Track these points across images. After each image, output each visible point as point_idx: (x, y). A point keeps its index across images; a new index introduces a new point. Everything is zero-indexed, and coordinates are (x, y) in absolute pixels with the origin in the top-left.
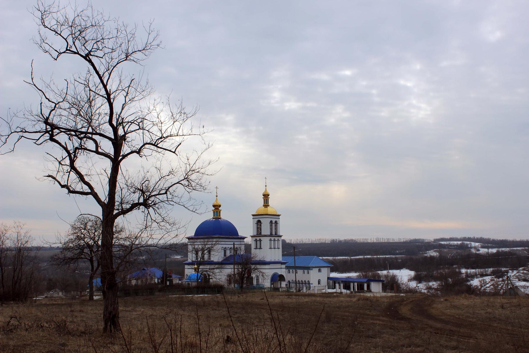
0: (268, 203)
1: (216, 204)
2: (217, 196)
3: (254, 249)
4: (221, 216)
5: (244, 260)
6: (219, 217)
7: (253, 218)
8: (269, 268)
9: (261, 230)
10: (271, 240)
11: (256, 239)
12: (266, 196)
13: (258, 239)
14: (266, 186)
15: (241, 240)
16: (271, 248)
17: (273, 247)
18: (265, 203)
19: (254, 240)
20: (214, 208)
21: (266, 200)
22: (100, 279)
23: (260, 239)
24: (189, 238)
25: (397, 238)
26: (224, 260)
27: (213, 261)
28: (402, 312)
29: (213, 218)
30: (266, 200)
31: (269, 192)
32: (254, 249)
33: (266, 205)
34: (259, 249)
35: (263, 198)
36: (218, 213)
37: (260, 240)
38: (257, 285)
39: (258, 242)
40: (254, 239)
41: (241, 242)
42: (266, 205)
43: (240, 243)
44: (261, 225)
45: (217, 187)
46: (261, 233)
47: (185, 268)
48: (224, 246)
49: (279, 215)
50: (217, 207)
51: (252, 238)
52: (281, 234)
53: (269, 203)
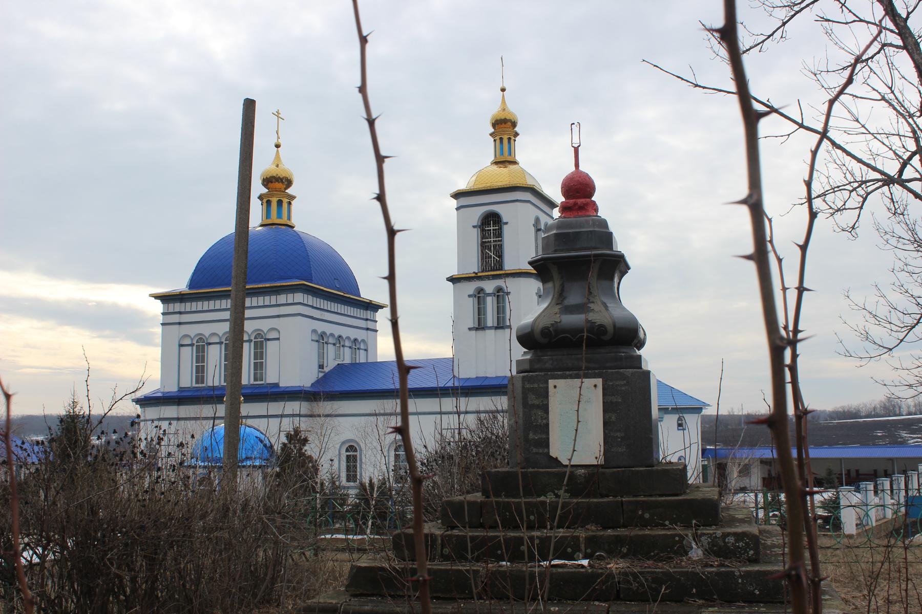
0: (289, 218)
1: (275, 172)
2: (278, 146)
3: (470, 329)
4: (294, 221)
7: (457, 209)
8: (368, 412)
9: (484, 246)
10: (480, 296)
11: (480, 290)
13: (489, 286)
15: (369, 314)
16: (480, 327)
17: (490, 320)
19: (471, 292)
22: (561, 383)
24: (146, 402)
26: (318, 382)
27: (276, 385)
31: (515, 109)
32: (470, 329)
33: (505, 160)
34: (497, 328)
35: (491, 135)
36: (285, 205)
37: (500, 294)
38: (73, 412)
39: (489, 300)
40: (471, 287)
41: (367, 320)
43: (363, 324)
44: (499, 234)
46: (499, 265)
48: (193, 330)
51: (458, 285)
53: (516, 156)
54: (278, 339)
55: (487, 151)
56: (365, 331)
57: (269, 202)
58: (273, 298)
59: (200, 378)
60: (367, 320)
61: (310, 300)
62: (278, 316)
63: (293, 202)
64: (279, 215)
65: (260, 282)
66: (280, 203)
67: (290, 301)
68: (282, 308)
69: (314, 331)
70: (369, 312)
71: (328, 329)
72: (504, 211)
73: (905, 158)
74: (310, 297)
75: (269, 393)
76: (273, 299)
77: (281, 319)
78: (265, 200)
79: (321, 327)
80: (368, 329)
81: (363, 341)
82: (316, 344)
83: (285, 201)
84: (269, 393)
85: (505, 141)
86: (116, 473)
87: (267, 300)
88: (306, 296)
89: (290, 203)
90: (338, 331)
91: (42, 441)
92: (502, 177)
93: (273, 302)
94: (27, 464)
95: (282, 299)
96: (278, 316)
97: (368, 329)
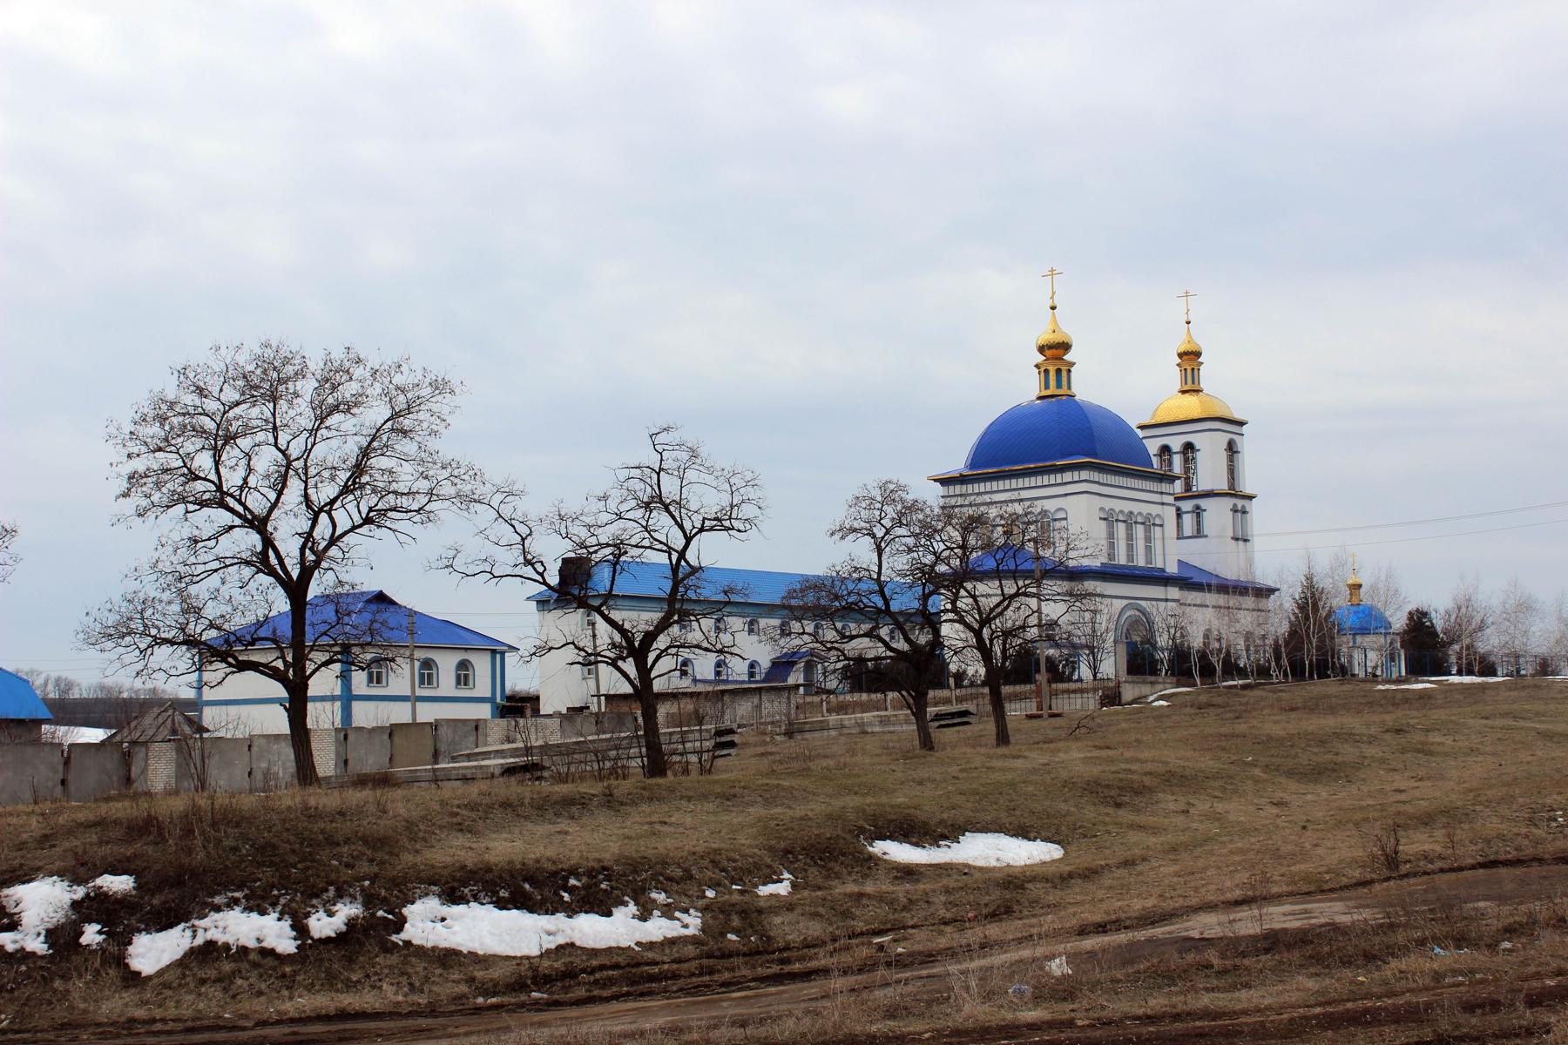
0: (1069, 388)
4: (1075, 389)
5: (695, 624)
6: (1069, 393)
12: (1190, 357)
13: (1187, 506)
14: (1188, 323)
18: (1052, 382)
20: (1040, 358)
21: (1193, 369)
23: (1198, 507)
25: (117, 599)
28: (1339, 759)
29: (1040, 398)
30: (1193, 369)
33: (1191, 387)
36: (1064, 374)
37: (1198, 511)
41: (1162, 493)
42: (1191, 387)
45: (1052, 270)
47: (310, 693)
49: (1241, 424)
50: (1056, 352)
52: (1248, 491)
54: (1065, 519)
55: (1174, 377)
56: (1160, 506)
57: (1046, 371)
58: (1059, 476)
59: (1130, 557)
60: (1162, 493)
61: (1096, 476)
62: (1066, 495)
63: (1072, 369)
64: (1059, 386)
65: (1045, 460)
66: (1059, 371)
67: (1076, 479)
68: (1068, 486)
69: (1102, 509)
70: (1163, 485)
71: (1118, 505)
72: (1195, 439)
73: (730, 678)
74: (1096, 474)
75: (370, 785)
76: (1059, 478)
77: (1068, 497)
78: (1042, 369)
79: (1109, 504)
80: (1163, 504)
81: (1158, 515)
82: (1104, 523)
83: (1064, 369)
84: (370, 785)
85: (1189, 372)
86: (597, 563)
87: (1052, 479)
88: (1092, 473)
89: (1069, 371)
90: (1127, 507)
91: (980, 979)
92: (1190, 406)
93: (1059, 481)
94: (1244, 957)
95: (1068, 476)
96: (1066, 495)
97: (1163, 504)
